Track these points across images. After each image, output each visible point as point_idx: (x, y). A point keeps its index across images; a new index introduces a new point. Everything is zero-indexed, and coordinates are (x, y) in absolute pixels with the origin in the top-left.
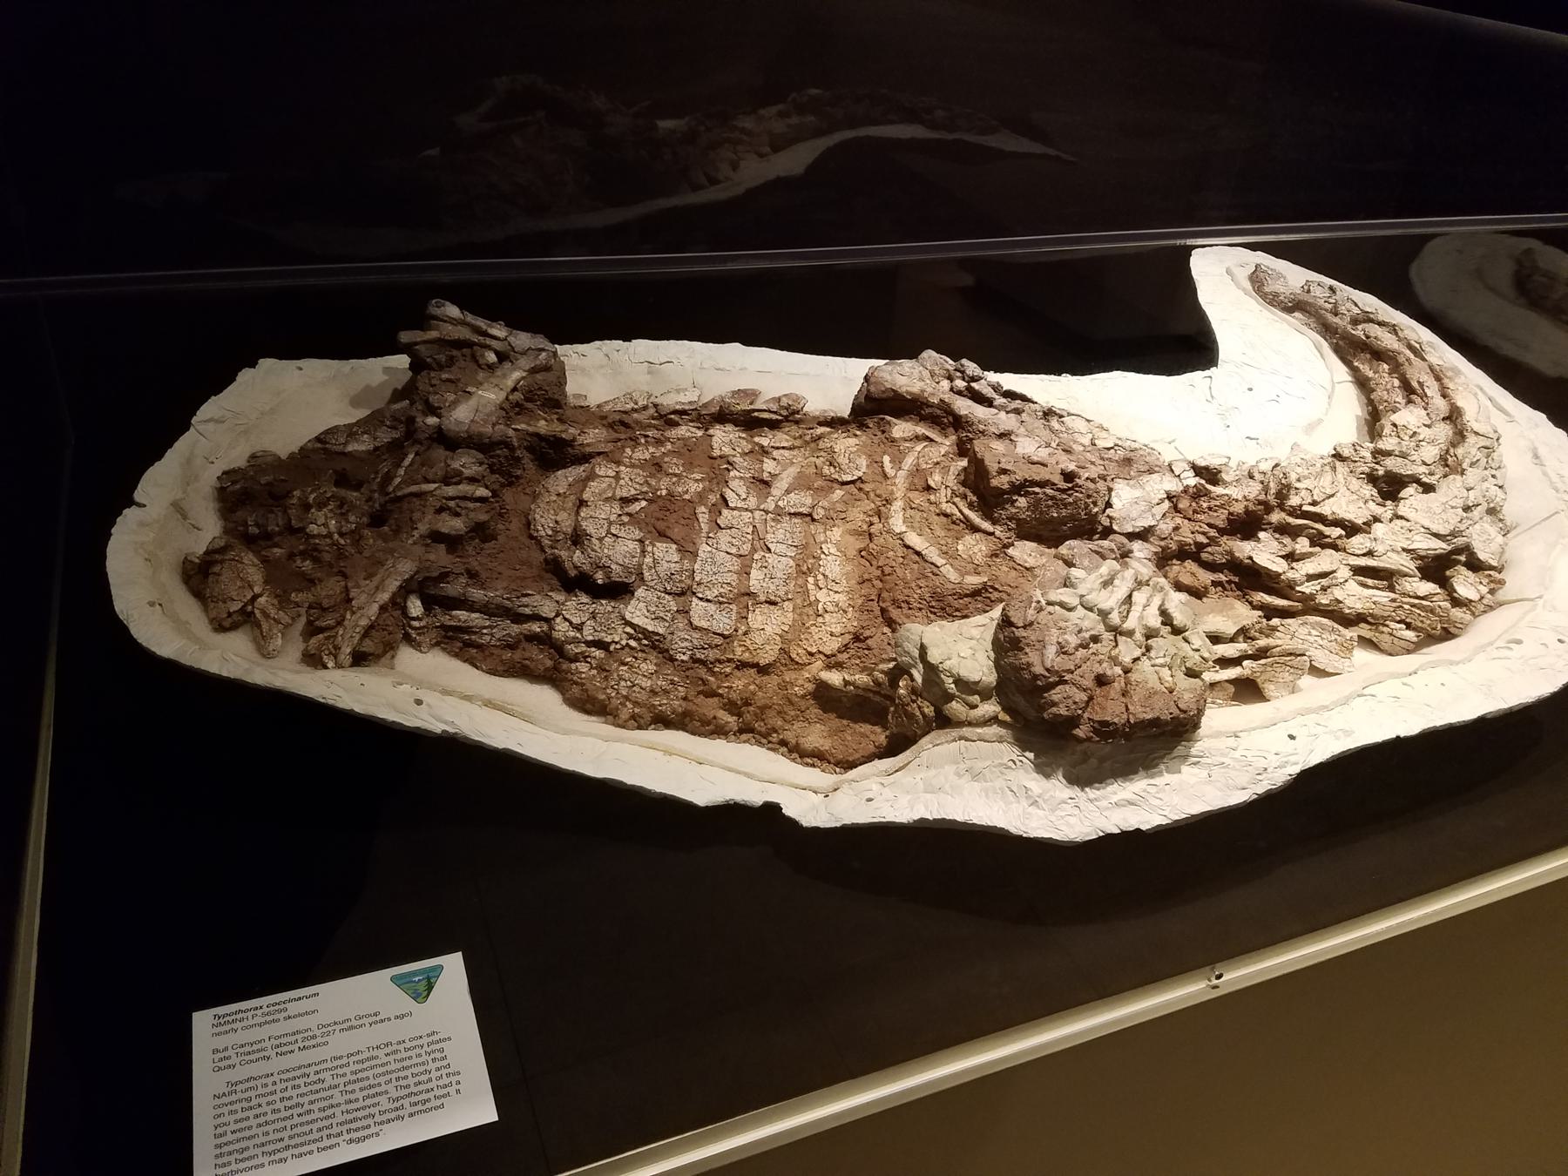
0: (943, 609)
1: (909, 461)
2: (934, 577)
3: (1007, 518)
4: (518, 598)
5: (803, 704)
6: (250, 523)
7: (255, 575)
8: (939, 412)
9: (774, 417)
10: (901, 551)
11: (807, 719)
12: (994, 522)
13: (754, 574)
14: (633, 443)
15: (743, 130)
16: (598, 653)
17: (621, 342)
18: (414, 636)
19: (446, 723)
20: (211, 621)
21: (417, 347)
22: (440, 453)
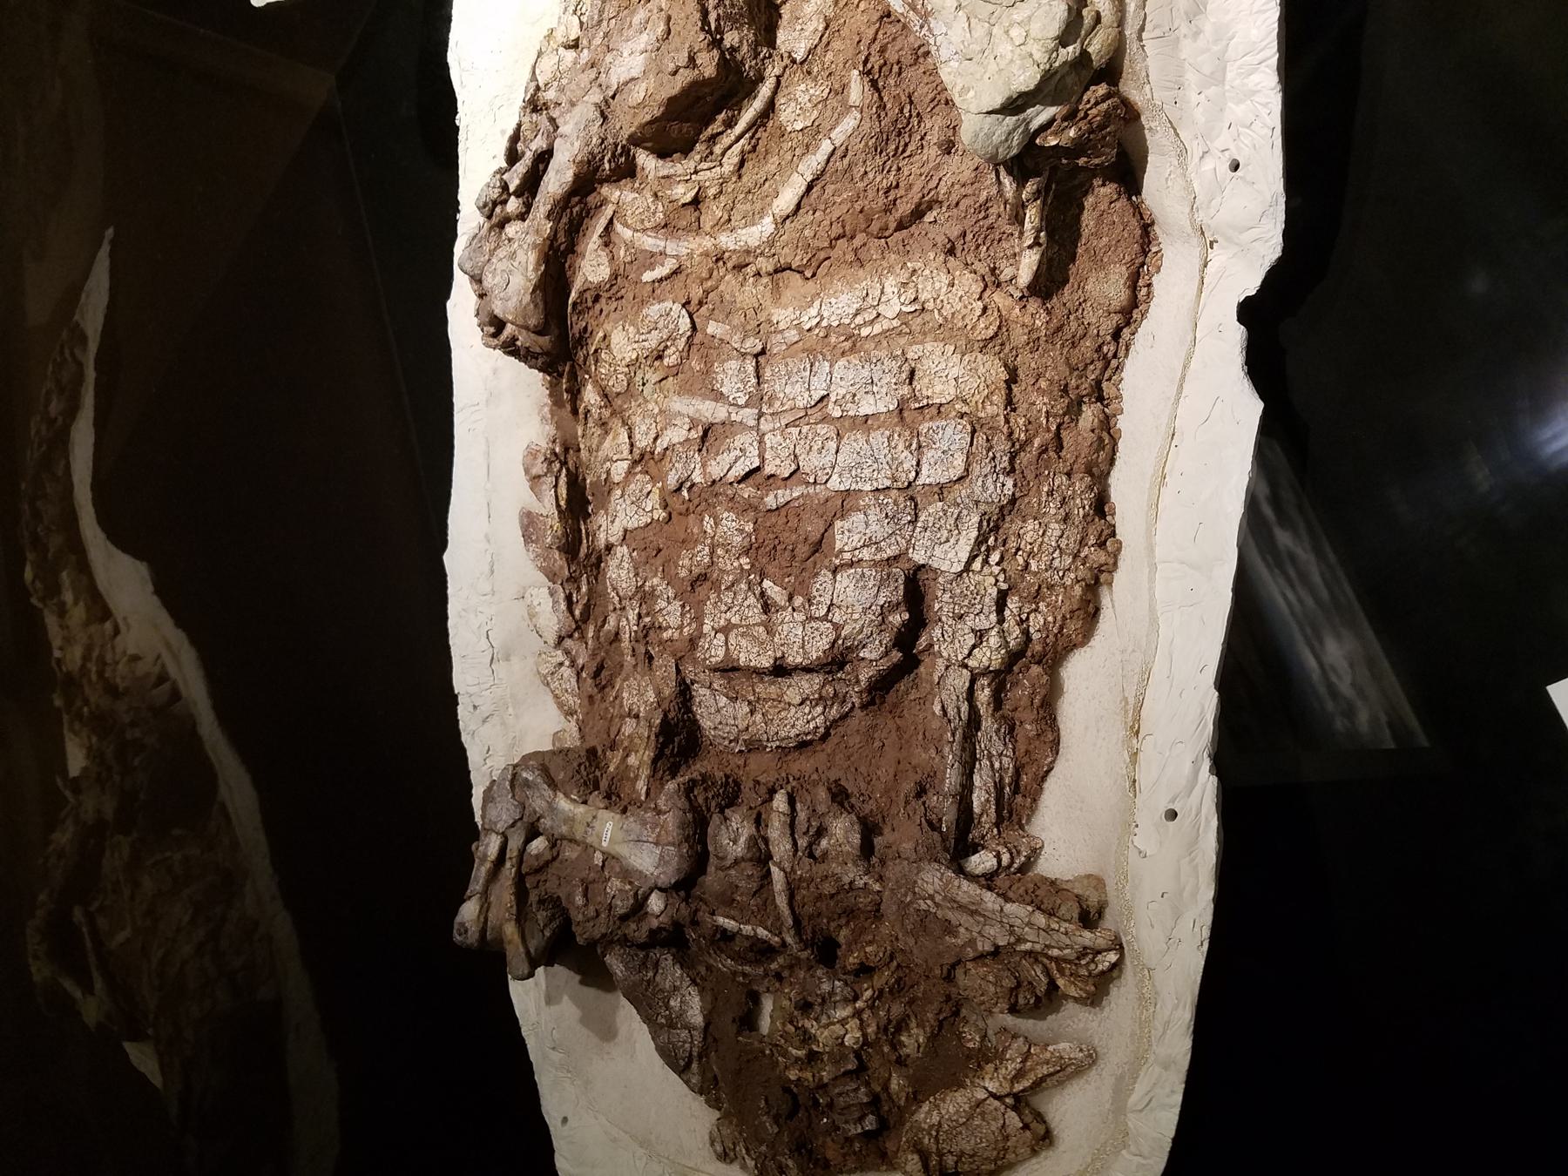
0: (899, 134)
1: (650, 242)
2: (850, 153)
3: (755, 58)
4: (949, 721)
5: (1059, 312)
6: (859, 1131)
7: (954, 1104)
8: (565, 220)
9: (563, 479)
10: (805, 218)
11: (1080, 304)
12: (761, 78)
13: (866, 407)
14: (651, 633)
15: (86, 658)
16: (1013, 604)
17: (459, 707)
18: (1023, 859)
19: (1196, 772)
20: (1035, 1152)
21: (532, 951)
22: (712, 879)
